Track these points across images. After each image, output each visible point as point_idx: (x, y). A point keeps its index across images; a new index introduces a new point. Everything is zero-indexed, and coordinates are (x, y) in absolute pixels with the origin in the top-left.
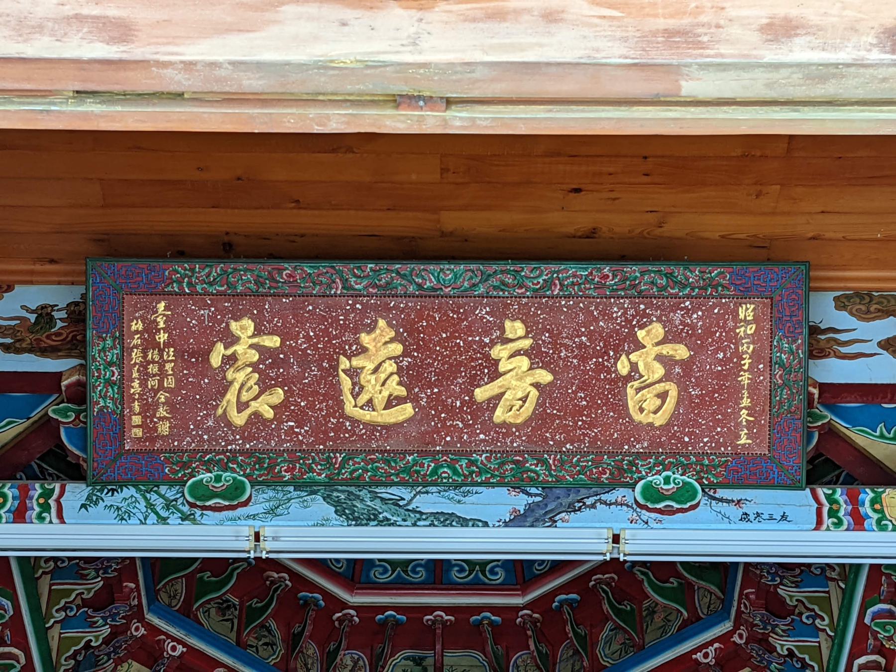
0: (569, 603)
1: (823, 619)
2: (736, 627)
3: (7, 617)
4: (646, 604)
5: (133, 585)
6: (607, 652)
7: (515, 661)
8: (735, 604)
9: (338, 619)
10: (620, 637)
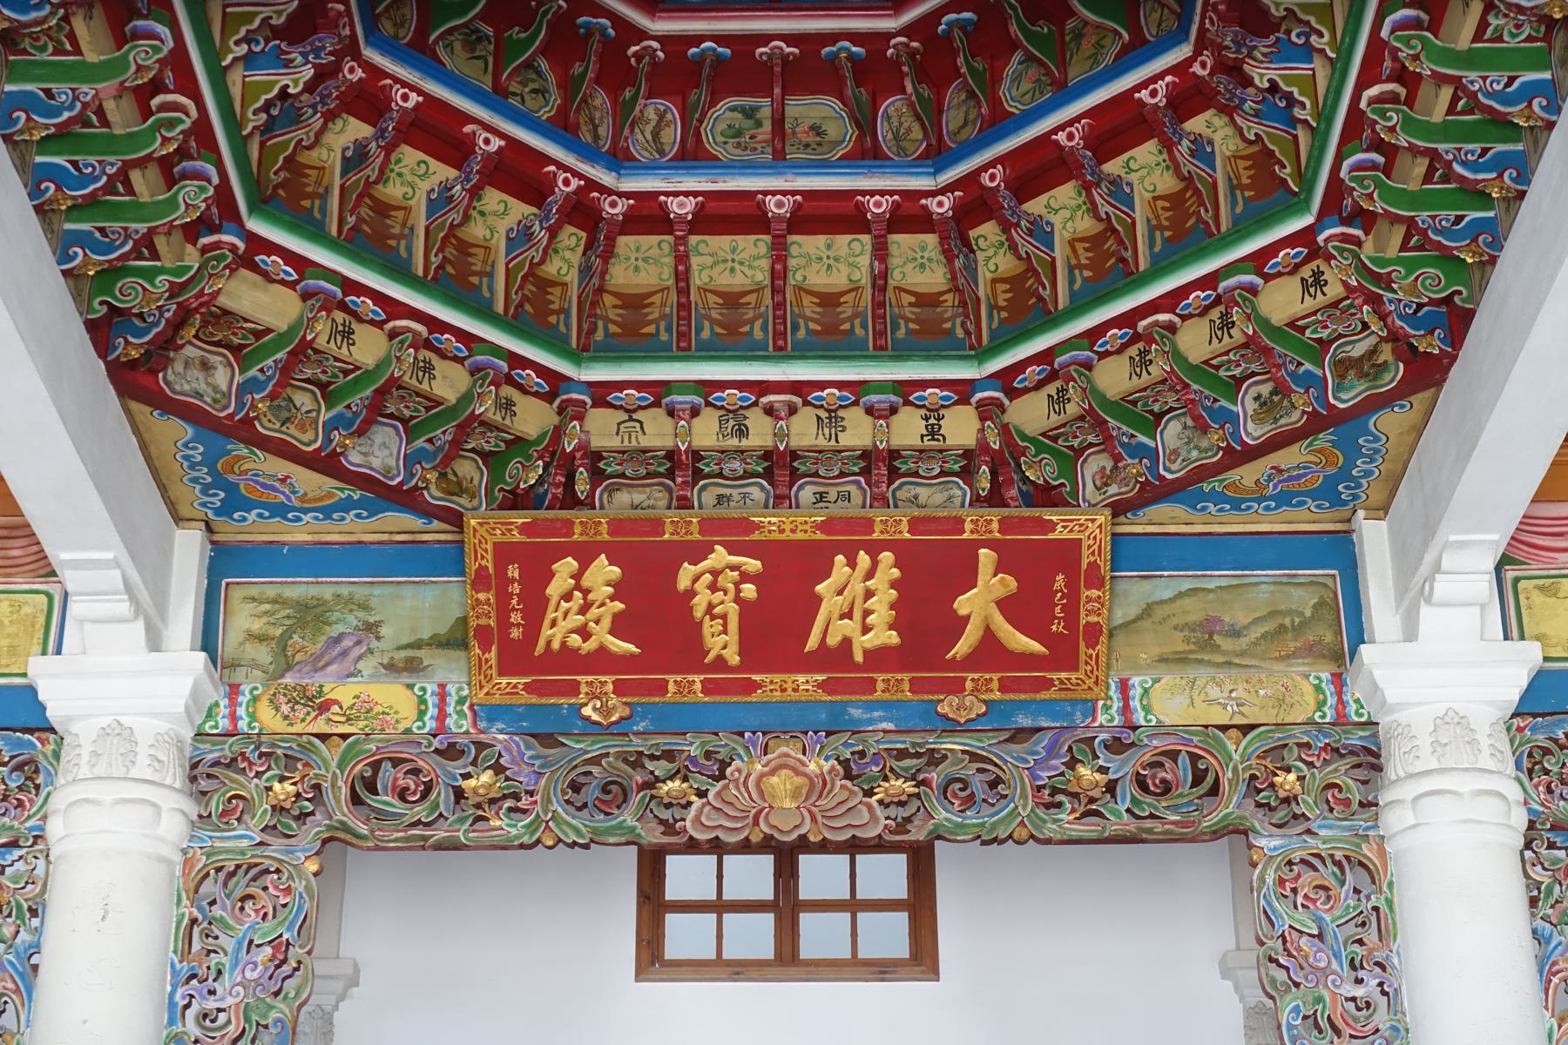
0: (962, 25)
1: (1321, 35)
2: (1197, 52)
3: (166, 50)
4: (1070, 24)
5: (341, 7)
6: (1014, 92)
7: (886, 110)
8: (1197, 19)
9: (635, 54)
10: (1034, 71)
